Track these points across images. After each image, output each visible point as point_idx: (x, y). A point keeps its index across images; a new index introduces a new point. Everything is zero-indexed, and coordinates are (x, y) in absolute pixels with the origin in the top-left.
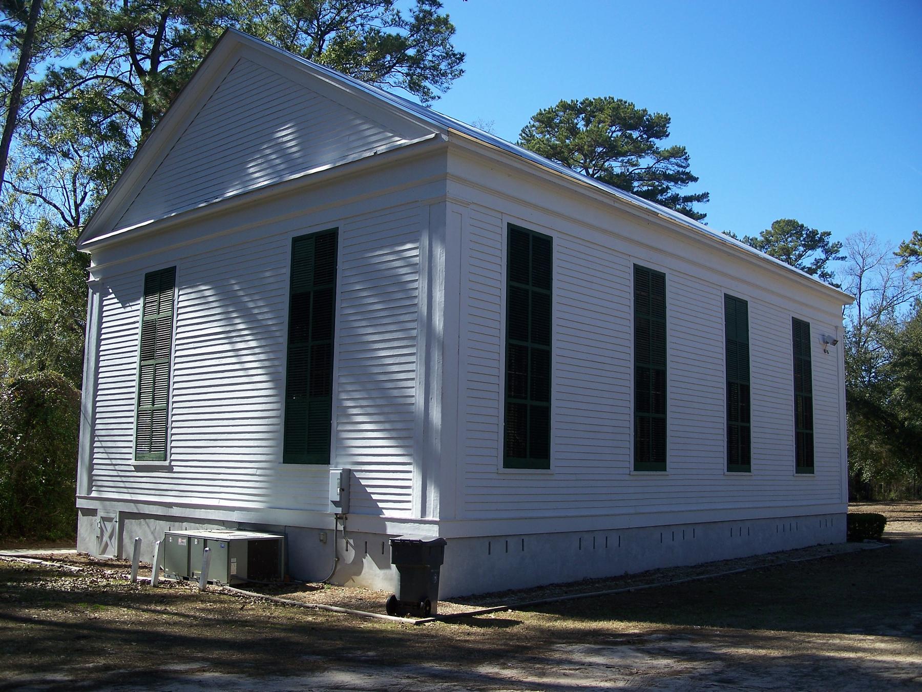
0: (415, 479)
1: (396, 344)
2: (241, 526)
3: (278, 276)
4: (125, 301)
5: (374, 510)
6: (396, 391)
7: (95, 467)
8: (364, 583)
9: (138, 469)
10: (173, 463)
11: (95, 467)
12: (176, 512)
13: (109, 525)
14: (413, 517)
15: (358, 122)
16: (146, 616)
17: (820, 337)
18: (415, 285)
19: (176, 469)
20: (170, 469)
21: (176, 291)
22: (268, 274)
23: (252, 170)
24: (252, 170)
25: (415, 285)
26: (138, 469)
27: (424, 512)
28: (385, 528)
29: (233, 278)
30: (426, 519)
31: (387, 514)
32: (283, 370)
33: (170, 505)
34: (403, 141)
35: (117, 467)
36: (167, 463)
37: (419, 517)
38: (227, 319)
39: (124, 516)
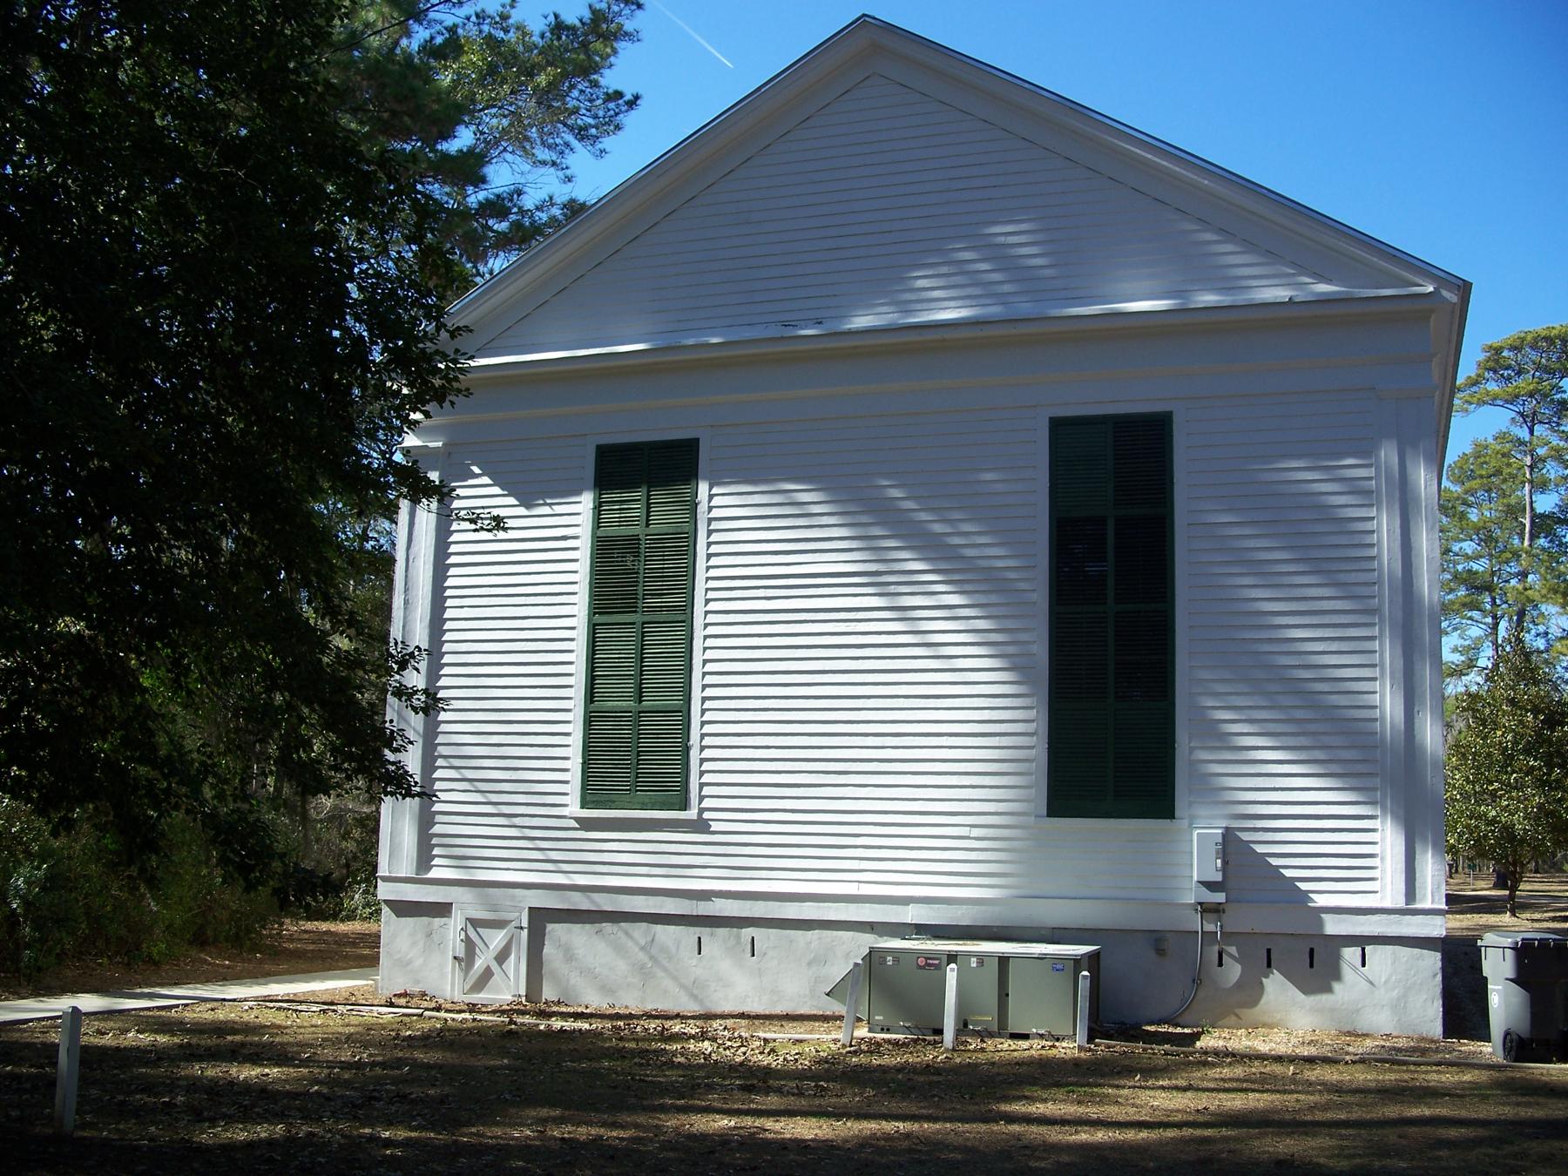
0: (1387, 839)
1: (1336, 619)
2: (921, 930)
3: (1026, 486)
4: (531, 488)
5: (1292, 896)
6: (1334, 697)
7: (438, 818)
8: (1266, 1019)
9: (586, 824)
10: (706, 815)
11: (438, 818)
12: (606, 903)
13: (497, 939)
14: (1387, 904)
15: (1209, 236)
16: (1406, 1076)
17: (551, 18)
18: (1368, 526)
19: (715, 826)
20: (701, 826)
21: (703, 488)
22: (989, 476)
23: (921, 283)
24: (921, 283)
25: (1368, 526)
26: (586, 824)
27: (1411, 893)
28: (1321, 923)
29: (887, 476)
30: (1418, 906)
31: (1321, 901)
32: (1040, 650)
33: (705, 895)
34: (1323, 288)
35: (517, 821)
36: (692, 814)
37: (1401, 903)
38: (868, 543)
39: (540, 918)
